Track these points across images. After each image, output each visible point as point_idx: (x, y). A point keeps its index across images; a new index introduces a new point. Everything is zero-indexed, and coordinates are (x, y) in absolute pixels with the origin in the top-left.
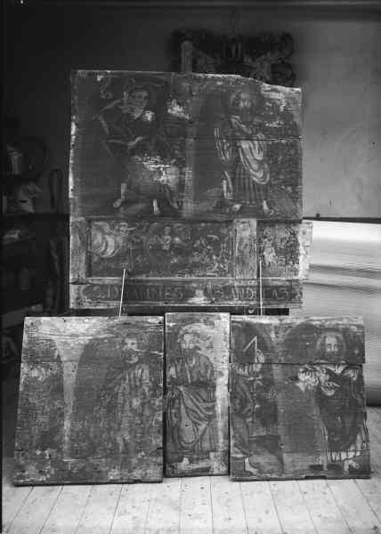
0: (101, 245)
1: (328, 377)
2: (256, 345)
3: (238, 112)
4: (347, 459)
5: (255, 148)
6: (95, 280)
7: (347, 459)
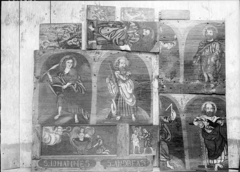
0: (48, 139)
1: (208, 124)
2: (172, 108)
3: (119, 69)
4: (217, 163)
5: (128, 87)
6: (44, 157)
7: (217, 163)
